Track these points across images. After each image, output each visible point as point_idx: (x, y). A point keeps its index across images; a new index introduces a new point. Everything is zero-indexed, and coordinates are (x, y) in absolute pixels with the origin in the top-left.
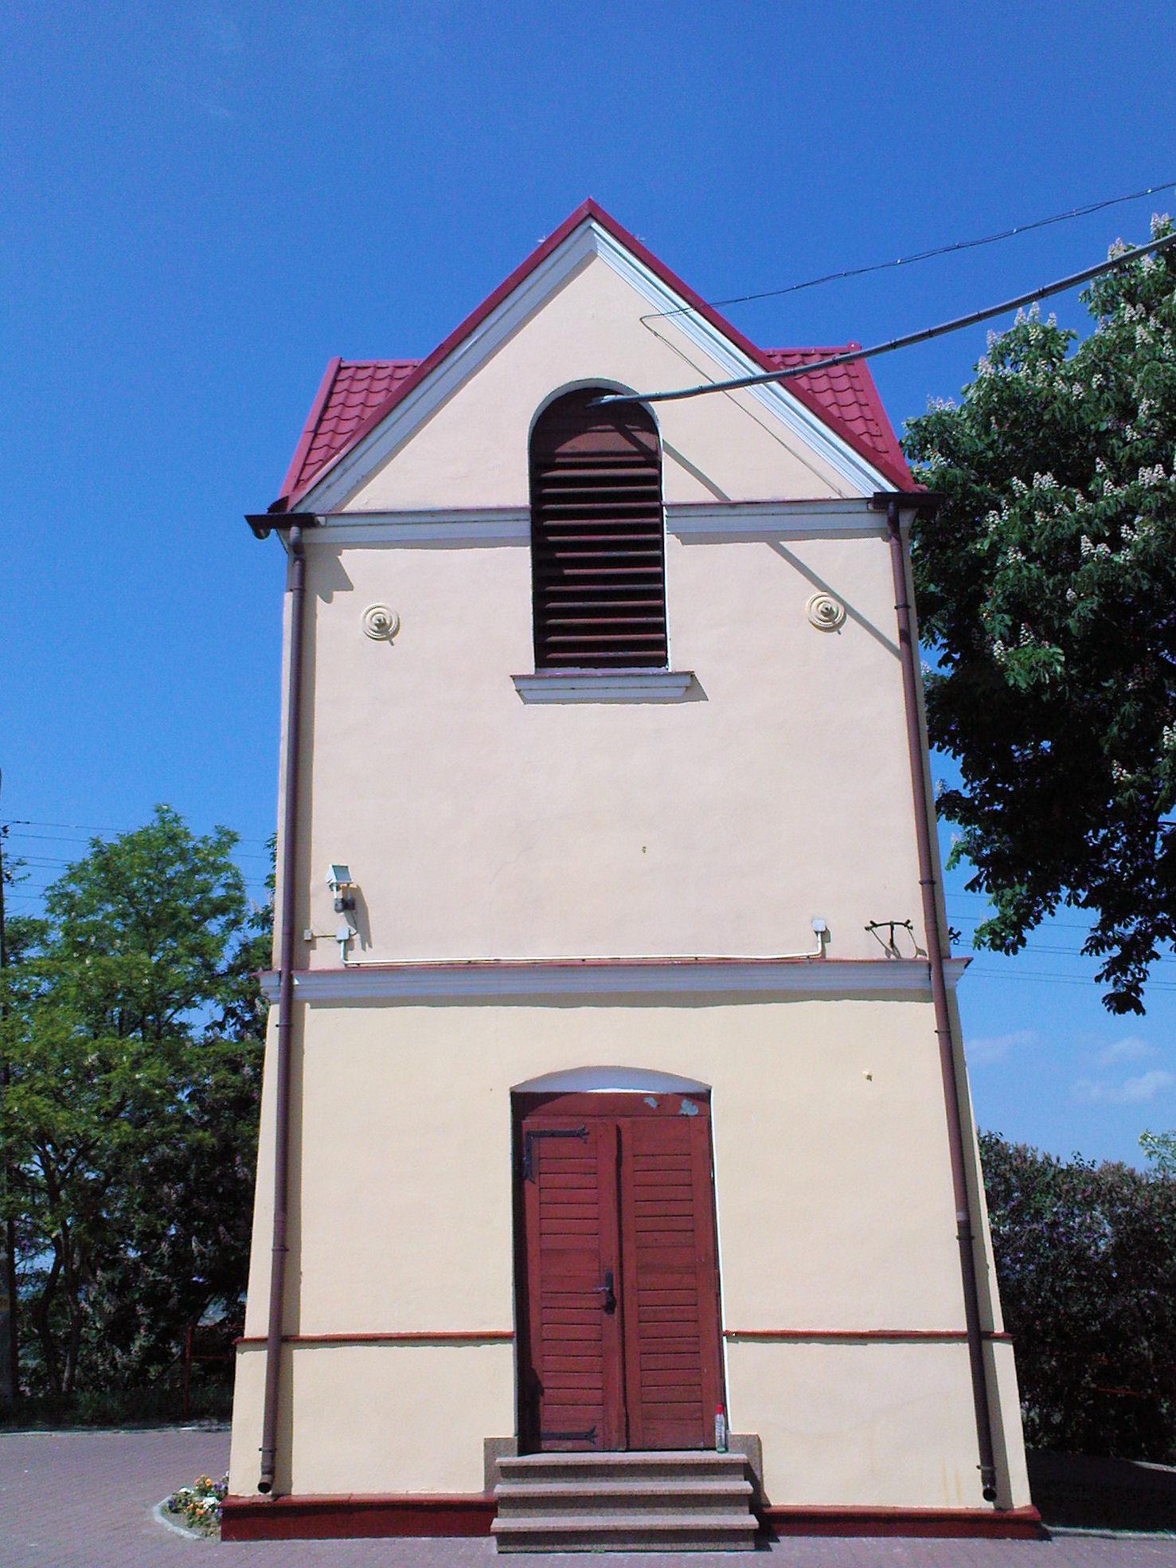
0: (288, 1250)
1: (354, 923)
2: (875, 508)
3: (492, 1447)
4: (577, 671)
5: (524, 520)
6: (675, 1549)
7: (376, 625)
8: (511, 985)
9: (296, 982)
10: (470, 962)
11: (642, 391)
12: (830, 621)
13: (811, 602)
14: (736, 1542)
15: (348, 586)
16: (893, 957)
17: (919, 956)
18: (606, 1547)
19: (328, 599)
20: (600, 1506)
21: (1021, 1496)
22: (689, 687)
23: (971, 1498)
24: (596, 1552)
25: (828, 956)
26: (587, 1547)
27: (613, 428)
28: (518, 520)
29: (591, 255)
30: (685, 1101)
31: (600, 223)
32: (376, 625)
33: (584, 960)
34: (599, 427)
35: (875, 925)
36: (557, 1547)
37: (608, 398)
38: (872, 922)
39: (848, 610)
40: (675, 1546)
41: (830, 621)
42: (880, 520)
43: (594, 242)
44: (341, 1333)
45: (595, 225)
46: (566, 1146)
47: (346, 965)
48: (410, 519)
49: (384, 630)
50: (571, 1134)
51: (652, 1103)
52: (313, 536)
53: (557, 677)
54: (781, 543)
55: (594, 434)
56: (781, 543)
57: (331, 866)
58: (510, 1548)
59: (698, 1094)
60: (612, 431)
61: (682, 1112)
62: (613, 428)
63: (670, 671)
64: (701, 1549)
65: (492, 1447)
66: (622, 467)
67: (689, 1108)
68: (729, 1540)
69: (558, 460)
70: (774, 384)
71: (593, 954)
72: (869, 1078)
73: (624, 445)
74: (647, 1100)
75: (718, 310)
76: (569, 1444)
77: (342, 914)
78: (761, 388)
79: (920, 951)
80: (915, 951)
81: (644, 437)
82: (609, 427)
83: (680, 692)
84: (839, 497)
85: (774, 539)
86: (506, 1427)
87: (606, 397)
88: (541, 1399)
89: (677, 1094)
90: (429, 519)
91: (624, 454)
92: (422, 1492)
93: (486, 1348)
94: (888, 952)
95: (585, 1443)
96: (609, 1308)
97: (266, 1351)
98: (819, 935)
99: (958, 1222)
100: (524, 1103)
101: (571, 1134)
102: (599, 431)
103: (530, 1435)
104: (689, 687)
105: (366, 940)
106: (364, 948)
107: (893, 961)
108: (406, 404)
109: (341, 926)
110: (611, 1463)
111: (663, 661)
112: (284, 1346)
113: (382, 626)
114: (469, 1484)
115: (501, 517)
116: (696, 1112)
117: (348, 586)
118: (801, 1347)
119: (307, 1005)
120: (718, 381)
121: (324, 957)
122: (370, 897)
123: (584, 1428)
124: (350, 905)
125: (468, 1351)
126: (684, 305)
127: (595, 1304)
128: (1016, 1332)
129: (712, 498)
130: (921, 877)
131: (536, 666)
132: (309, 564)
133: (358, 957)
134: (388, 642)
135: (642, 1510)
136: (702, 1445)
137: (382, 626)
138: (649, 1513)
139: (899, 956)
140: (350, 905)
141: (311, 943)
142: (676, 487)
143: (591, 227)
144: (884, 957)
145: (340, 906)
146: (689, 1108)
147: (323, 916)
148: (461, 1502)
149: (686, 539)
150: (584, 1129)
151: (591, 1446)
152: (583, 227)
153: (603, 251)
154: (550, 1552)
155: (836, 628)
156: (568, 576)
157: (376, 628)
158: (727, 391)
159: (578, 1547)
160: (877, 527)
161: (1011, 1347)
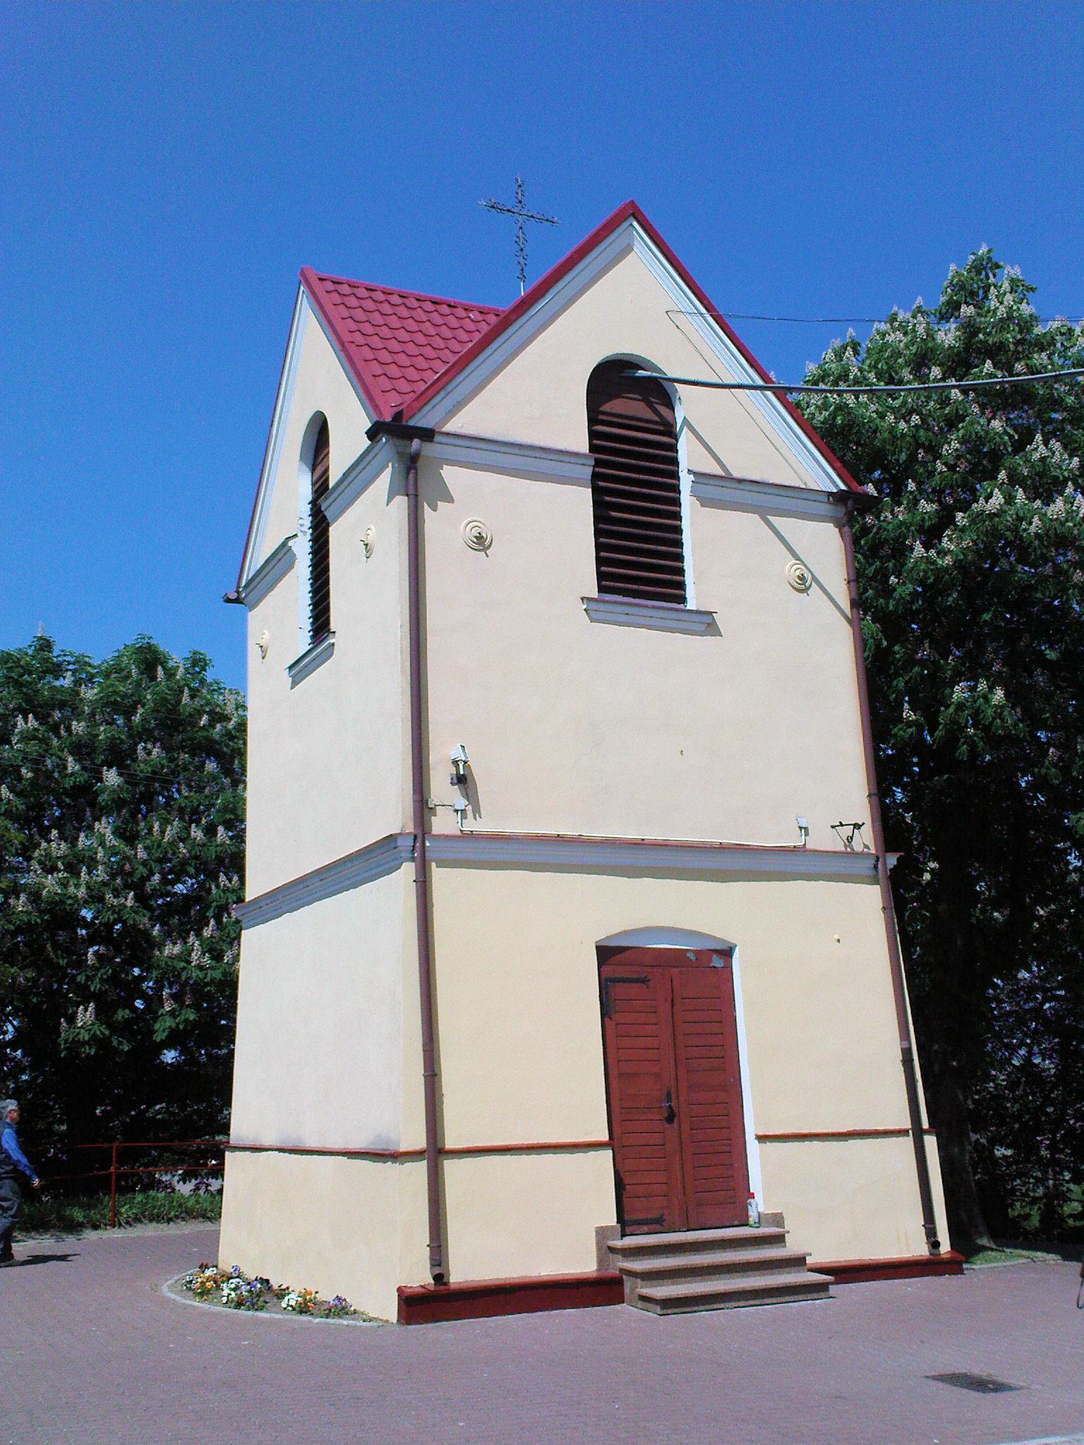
0: (436, 1075)
1: (466, 795)
2: (834, 501)
3: (602, 1233)
4: (620, 598)
5: (589, 466)
6: (779, 1301)
7: (476, 537)
8: (591, 857)
9: (428, 844)
10: (558, 835)
11: (671, 370)
12: (802, 585)
13: (791, 569)
14: (818, 1293)
15: (450, 500)
16: (849, 850)
17: (865, 850)
18: (734, 1304)
19: (434, 509)
20: (709, 1274)
21: (945, 1247)
22: (706, 624)
23: (920, 1250)
24: (728, 1308)
25: (807, 847)
26: (722, 1306)
27: (640, 398)
28: (584, 465)
29: (628, 249)
30: (715, 956)
31: (639, 222)
32: (476, 537)
33: (643, 840)
34: (630, 395)
35: (842, 825)
36: (702, 1308)
37: (641, 373)
38: (840, 822)
39: (814, 578)
40: (779, 1300)
41: (802, 585)
42: (840, 511)
43: (632, 239)
44: (593, 1140)
45: (635, 224)
46: (635, 989)
47: (461, 831)
48: (503, 449)
49: (481, 543)
50: (637, 981)
51: (692, 956)
52: (429, 450)
53: (647, 607)
54: (768, 517)
55: (625, 400)
56: (768, 517)
57: (459, 745)
58: (669, 1311)
59: (723, 950)
60: (639, 400)
61: (712, 965)
62: (640, 398)
63: (688, 608)
64: (796, 1300)
65: (602, 1233)
66: (607, 425)
67: (717, 962)
68: (814, 1291)
69: (602, 417)
70: (769, 393)
71: (650, 835)
72: (839, 941)
73: (649, 415)
74: (688, 955)
75: (727, 320)
76: (646, 1228)
77: (456, 787)
78: (757, 393)
79: (866, 846)
80: (862, 846)
81: (663, 410)
82: (636, 396)
83: (703, 627)
84: (804, 487)
85: (764, 512)
86: (611, 1219)
87: (640, 371)
88: (624, 1192)
89: (710, 950)
90: (516, 451)
91: (647, 421)
92: (551, 1273)
93: (592, 1154)
94: (846, 846)
95: (658, 1227)
96: (671, 1118)
97: (425, 1162)
98: (803, 830)
99: (902, 1049)
100: (605, 953)
101: (637, 981)
102: (631, 399)
103: (625, 1222)
104: (706, 624)
105: (477, 811)
106: (475, 819)
107: (848, 853)
108: (494, 346)
109: (455, 797)
110: (700, 1240)
111: (683, 600)
112: (442, 1157)
113: (480, 538)
114: (584, 1264)
115: (573, 460)
116: (722, 965)
117: (450, 500)
118: (807, 1144)
119: (433, 865)
120: (726, 382)
121: (442, 823)
122: (478, 773)
123: (655, 1214)
124: (462, 780)
125: (579, 1157)
126: (703, 311)
127: (658, 1117)
128: (935, 1127)
129: (721, 473)
130: (869, 789)
131: (599, 592)
132: (420, 473)
133: (471, 825)
134: (483, 553)
135: (738, 1274)
136: (736, 1223)
137: (480, 538)
138: (743, 1277)
139: (853, 850)
140: (462, 780)
141: (432, 810)
142: (688, 455)
143: (631, 225)
144: (843, 849)
145: (455, 781)
146: (717, 962)
147: (441, 789)
148: (577, 1279)
149: (705, 502)
150: (646, 977)
151: (661, 1228)
152: (625, 225)
153: (638, 247)
154: (695, 1312)
155: (805, 591)
156: (614, 517)
157: (475, 540)
158: (731, 390)
159: (715, 1306)
160: (830, 514)
161: (935, 1138)
